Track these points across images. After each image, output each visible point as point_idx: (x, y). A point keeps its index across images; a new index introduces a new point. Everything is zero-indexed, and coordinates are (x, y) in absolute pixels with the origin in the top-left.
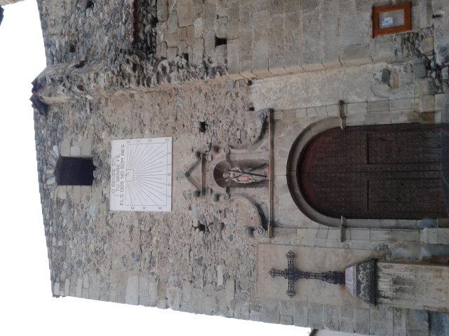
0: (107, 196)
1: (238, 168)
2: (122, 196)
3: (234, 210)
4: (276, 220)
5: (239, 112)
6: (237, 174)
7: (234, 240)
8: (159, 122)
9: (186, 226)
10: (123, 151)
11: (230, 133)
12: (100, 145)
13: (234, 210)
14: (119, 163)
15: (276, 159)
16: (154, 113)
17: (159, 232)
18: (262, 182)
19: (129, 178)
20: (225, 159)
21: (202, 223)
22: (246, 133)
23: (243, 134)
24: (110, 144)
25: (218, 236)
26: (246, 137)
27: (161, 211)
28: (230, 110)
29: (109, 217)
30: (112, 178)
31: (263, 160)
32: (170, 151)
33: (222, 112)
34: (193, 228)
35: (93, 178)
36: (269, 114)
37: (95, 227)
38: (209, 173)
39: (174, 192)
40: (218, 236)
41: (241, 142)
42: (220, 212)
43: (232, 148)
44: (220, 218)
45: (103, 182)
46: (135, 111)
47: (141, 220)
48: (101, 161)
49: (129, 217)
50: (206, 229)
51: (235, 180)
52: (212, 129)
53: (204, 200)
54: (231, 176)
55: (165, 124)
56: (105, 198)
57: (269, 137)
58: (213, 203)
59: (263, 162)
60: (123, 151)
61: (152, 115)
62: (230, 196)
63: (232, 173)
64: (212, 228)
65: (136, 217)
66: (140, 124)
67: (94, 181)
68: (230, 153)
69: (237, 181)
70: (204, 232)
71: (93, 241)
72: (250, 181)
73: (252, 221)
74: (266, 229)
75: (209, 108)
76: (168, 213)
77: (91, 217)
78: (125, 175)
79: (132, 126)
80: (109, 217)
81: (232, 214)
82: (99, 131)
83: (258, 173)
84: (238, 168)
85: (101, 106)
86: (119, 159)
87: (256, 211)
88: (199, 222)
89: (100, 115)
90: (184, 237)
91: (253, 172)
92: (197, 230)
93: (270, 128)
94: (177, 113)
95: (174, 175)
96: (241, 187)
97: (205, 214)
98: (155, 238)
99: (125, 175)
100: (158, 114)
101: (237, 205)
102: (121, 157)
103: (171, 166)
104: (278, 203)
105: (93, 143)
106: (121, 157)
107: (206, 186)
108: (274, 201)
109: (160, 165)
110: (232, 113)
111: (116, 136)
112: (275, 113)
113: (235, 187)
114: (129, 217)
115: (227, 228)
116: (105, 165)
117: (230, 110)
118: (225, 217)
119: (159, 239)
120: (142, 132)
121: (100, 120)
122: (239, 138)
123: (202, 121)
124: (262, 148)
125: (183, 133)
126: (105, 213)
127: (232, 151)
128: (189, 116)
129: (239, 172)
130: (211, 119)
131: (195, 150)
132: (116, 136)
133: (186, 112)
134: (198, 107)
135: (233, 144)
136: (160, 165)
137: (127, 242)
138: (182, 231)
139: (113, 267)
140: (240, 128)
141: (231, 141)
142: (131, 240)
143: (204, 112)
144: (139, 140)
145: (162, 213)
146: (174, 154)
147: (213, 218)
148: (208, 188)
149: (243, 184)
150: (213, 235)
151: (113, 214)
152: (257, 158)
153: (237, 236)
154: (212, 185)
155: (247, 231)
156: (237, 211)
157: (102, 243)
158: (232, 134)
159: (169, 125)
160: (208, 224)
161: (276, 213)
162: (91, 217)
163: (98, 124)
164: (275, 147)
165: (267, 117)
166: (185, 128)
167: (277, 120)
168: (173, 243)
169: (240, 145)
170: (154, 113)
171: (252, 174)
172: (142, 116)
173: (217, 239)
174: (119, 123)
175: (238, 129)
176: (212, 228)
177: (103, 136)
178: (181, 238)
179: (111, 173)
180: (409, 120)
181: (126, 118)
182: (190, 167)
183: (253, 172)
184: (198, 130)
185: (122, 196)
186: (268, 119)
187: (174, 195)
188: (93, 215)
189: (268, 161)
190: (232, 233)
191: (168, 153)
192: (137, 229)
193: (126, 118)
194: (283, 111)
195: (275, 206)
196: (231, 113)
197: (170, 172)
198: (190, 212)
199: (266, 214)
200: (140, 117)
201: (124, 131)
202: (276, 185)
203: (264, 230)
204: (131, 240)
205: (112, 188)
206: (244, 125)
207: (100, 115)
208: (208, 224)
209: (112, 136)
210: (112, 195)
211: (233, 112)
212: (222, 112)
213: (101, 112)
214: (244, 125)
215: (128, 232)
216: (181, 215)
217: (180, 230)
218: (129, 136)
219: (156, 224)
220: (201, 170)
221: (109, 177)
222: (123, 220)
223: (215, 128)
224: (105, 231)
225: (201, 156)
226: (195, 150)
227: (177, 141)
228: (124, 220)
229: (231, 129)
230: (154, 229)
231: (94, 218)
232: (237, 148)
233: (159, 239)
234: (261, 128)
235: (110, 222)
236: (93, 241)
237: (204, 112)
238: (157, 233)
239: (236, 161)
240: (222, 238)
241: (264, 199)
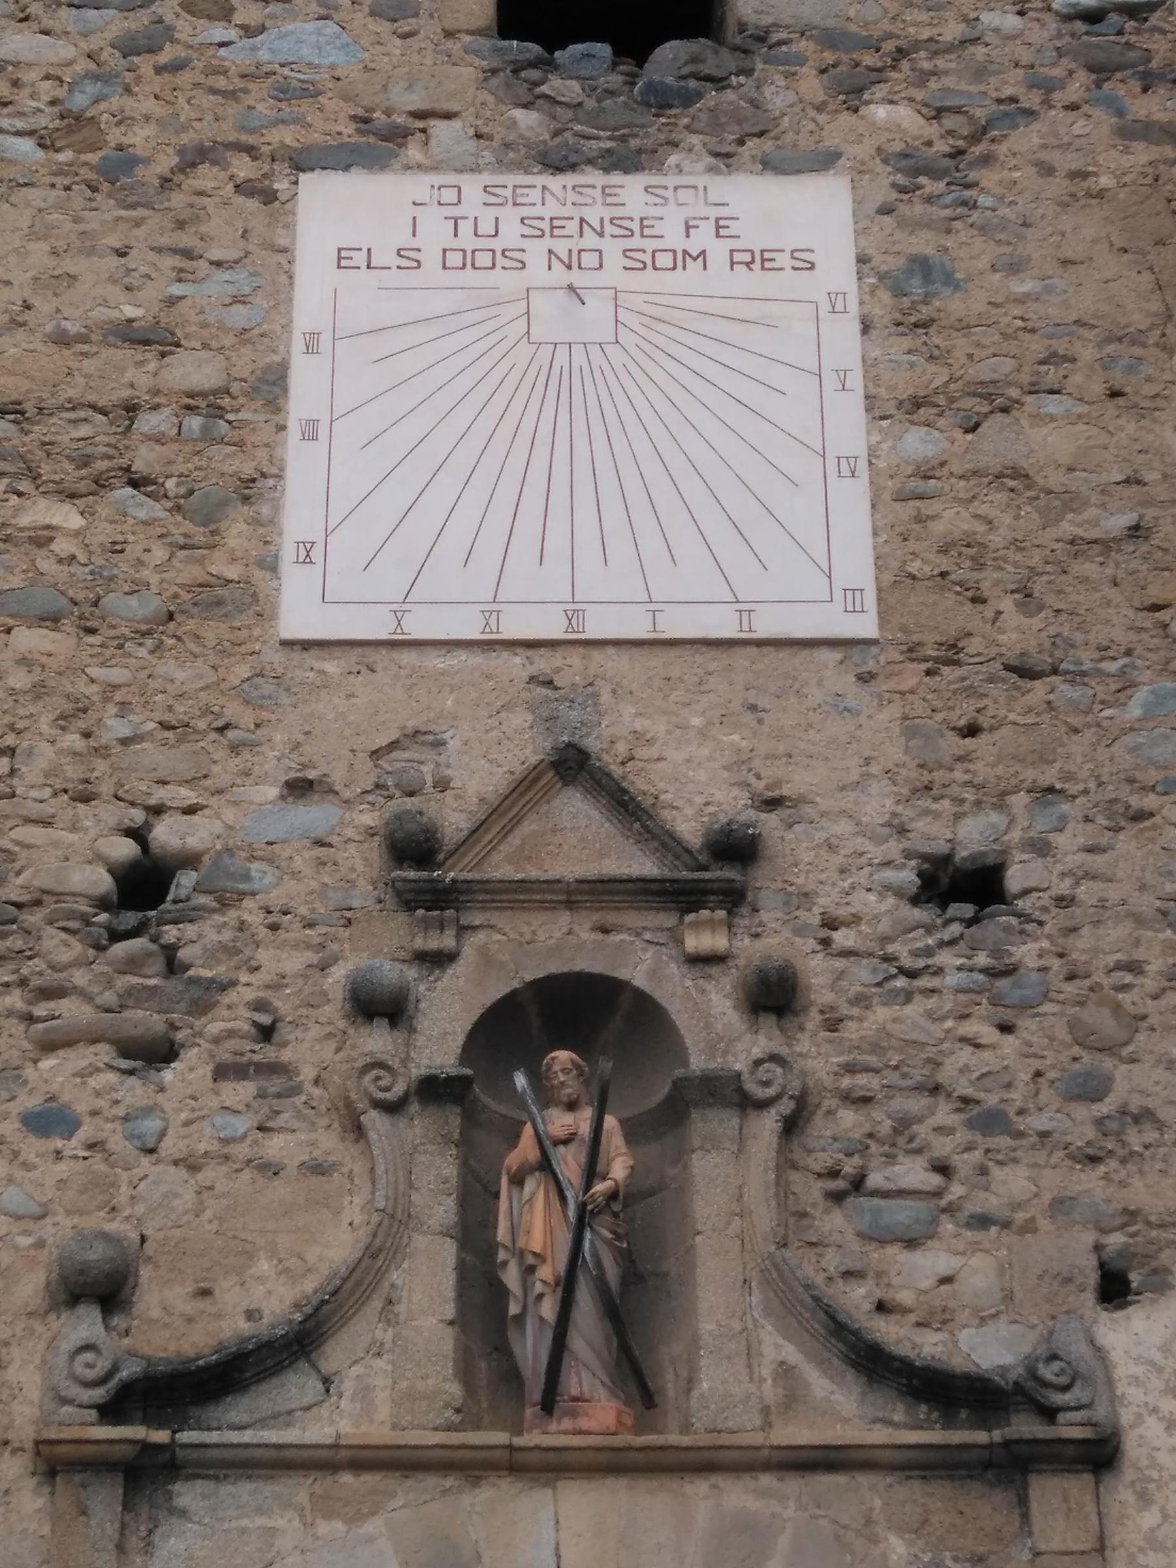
0: (413, 152)
1: (619, 1169)
2: (408, 258)
3: (274, 1147)
4: (187, 1494)
5: (1089, 1181)
6: (569, 1164)
7: (33, 1147)
8: (996, 540)
9: (150, 754)
10: (762, 260)
11: (916, 1104)
12: (811, 85)
13: (274, 1147)
14: (674, 237)
15: (698, 1488)
16: (1071, 502)
17: (117, 548)
18: (512, 1377)
19: (546, 306)
20: (698, 1063)
21: (185, 881)
22: (911, 1244)
23: (901, 1213)
24: (825, 161)
25: (71, 1010)
26: (879, 1237)
27: (288, 554)
28: (1103, 1108)
29: (243, 168)
30: (555, 183)
31: (691, 1381)
32: (767, 626)
33: (1083, 1037)
34: (138, 816)
35: (554, 43)
36: (1069, 1429)
37: (177, 67)
38: (586, 935)
39: (436, 661)
40: (71, 1010)
41: (837, 1197)
42: (266, 1033)
43: (791, 1126)
44: (215, 1028)
45: (519, 114)
46: (1087, 354)
47: (217, 412)
48: (688, 99)
49: (239, 316)
50: (130, 919)
51: (526, 1149)
52: (944, 958)
53: (363, 895)
54: (559, 1122)
55: (987, 581)
56: (397, 136)
57: (880, 1435)
58: (339, 973)
59: (669, 1384)
60: (762, 260)
61: (1056, 479)
62: (392, 1108)
63: (583, 1120)
64: (132, 965)
65: (245, 363)
66: (986, 391)
67: (534, 49)
68: (748, 1104)
69: (513, 1160)
70: (103, 904)
71: (65, 51)
72: (511, 1277)
73: (179, 1296)
74: (110, 1412)
75: (1116, 933)
76: (266, 614)
77: (249, 31)
78: (577, 278)
79: (963, 327)
80: (243, 168)
81: (242, 1124)
82: (923, 77)
83: (577, 1343)
84: (619, 1169)
85: (1123, 89)
86: (703, 237)
87: (263, 1328)
88: (190, 860)
89: (1048, 87)
90: (72, 740)
91: (585, 1299)
92: (126, 849)
93: (958, 1437)
94: (1077, 677)
95: (574, 658)
96: (464, 1203)
97: (250, 913)
98: (68, 517)
99: (577, 278)
100: (1067, 528)
101: (318, 1169)
102: (718, 251)
103: (640, 630)
104: (326, 1507)
105: (830, 39)
106: (718, 251)
107: (476, 918)
108: (346, 1478)
109: (652, 546)
110: (118, 696)
111: (886, 210)
112: (1078, 1486)
113: (466, 1145)
114: (239, 316)
115: (135, 1092)
116: (654, 129)
117: (1103, 1108)
118: (222, 1072)
119: (62, 546)
120: (917, 403)
121: (1011, 84)
122: (875, 1180)
123: (1014, 879)
124: (785, 1371)
125: (910, 728)
126: (287, 136)
127: (768, 1125)
128: (1049, 776)
129: (591, 1173)
130: (1026, 952)
131: (770, 822)
132: (886, 210)
133: (1078, 746)
134: (1125, 842)
135: (820, 1129)
136: (652, 546)
137: (44, 306)
138: (116, 727)
139: (199, 116)
140: (957, 1190)
141: (848, 1117)
142: (62, 340)
143: (1086, 892)
144: (856, 380)
145: (272, 567)
146: (741, 658)
147: (219, 971)
148: (463, 930)
149: (491, 1224)
150: (80, 978)
151: (269, 197)
152: (707, 1327)
153: (62, 1169)
154: (487, 959)
155: (96, 1254)
156: (271, 1170)
157: (46, 121)
158: (903, 1124)
159: (966, 616)
160: (171, 933)
161: (245, 1490)
162: (249, 31)
163: (981, 72)
164: (794, 1485)
165: (1049, 1414)
166: (953, 744)
167: (1023, 1501)
168: (24, 661)
169: (812, 1192)
170: (1071, 502)
171: (567, 1286)
172: (1053, 405)
173: (40, 1010)
174: (983, 229)
175: (943, 1169)
176: (132, 965)
177: (880, 112)
178: (63, 721)
179: (594, 177)
180: (169, 1496)
181: (1024, 286)
182: (638, 784)
183: (585, 1299)
184: (940, 847)
185: (408, 258)
186: (1026, 1427)
187: (408, 657)
188: (266, 49)
189: (686, 1428)
190: (82, 1134)
191: (744, 610)
192: (144, 381)
193: (1024, 286)
194: (1101, 1547)
195: (300, 1489)
196: (1082, 1112)
197: (593, 632)
198: (273, 792)
199: (238, 1408)
200: (1033, 390)
201: (922, 266)
202: (485, 1494)
203: (98, 1394)
204: (62, 340)
205: (472, 186)
206: (982, 1221)
207: (1048, 87)
208: (171, 933)
209: (881, 190)
210: (420, 186)
211: (1082, 1134)
212: (1083, 1037)
213: (1075, 90)
214: (982, 1221)
215: (130, 311)
216: (247, 718)
217: (124, 708)
218: (883, 306)
219: (181, 527)
220: (612, 867)
221: (557, 163)
222: (224, 275)
223: (952, 979)
224: (140, 138)
225: (728, 873)
226: (770, 822)
227: (847, 682)
228: (218, 285)
229: (944, 1114)
230: (144, 508)
231: (237, 57)
232: (785, 1164)
233: (62, 546)
234: (958, 1364)
235: (206, 177)
236: (65, 51)
237: (1086, 892)
238: (104, 533)
239: (681, 1155)
240: (49, 1046)
241: (365, 1393)
